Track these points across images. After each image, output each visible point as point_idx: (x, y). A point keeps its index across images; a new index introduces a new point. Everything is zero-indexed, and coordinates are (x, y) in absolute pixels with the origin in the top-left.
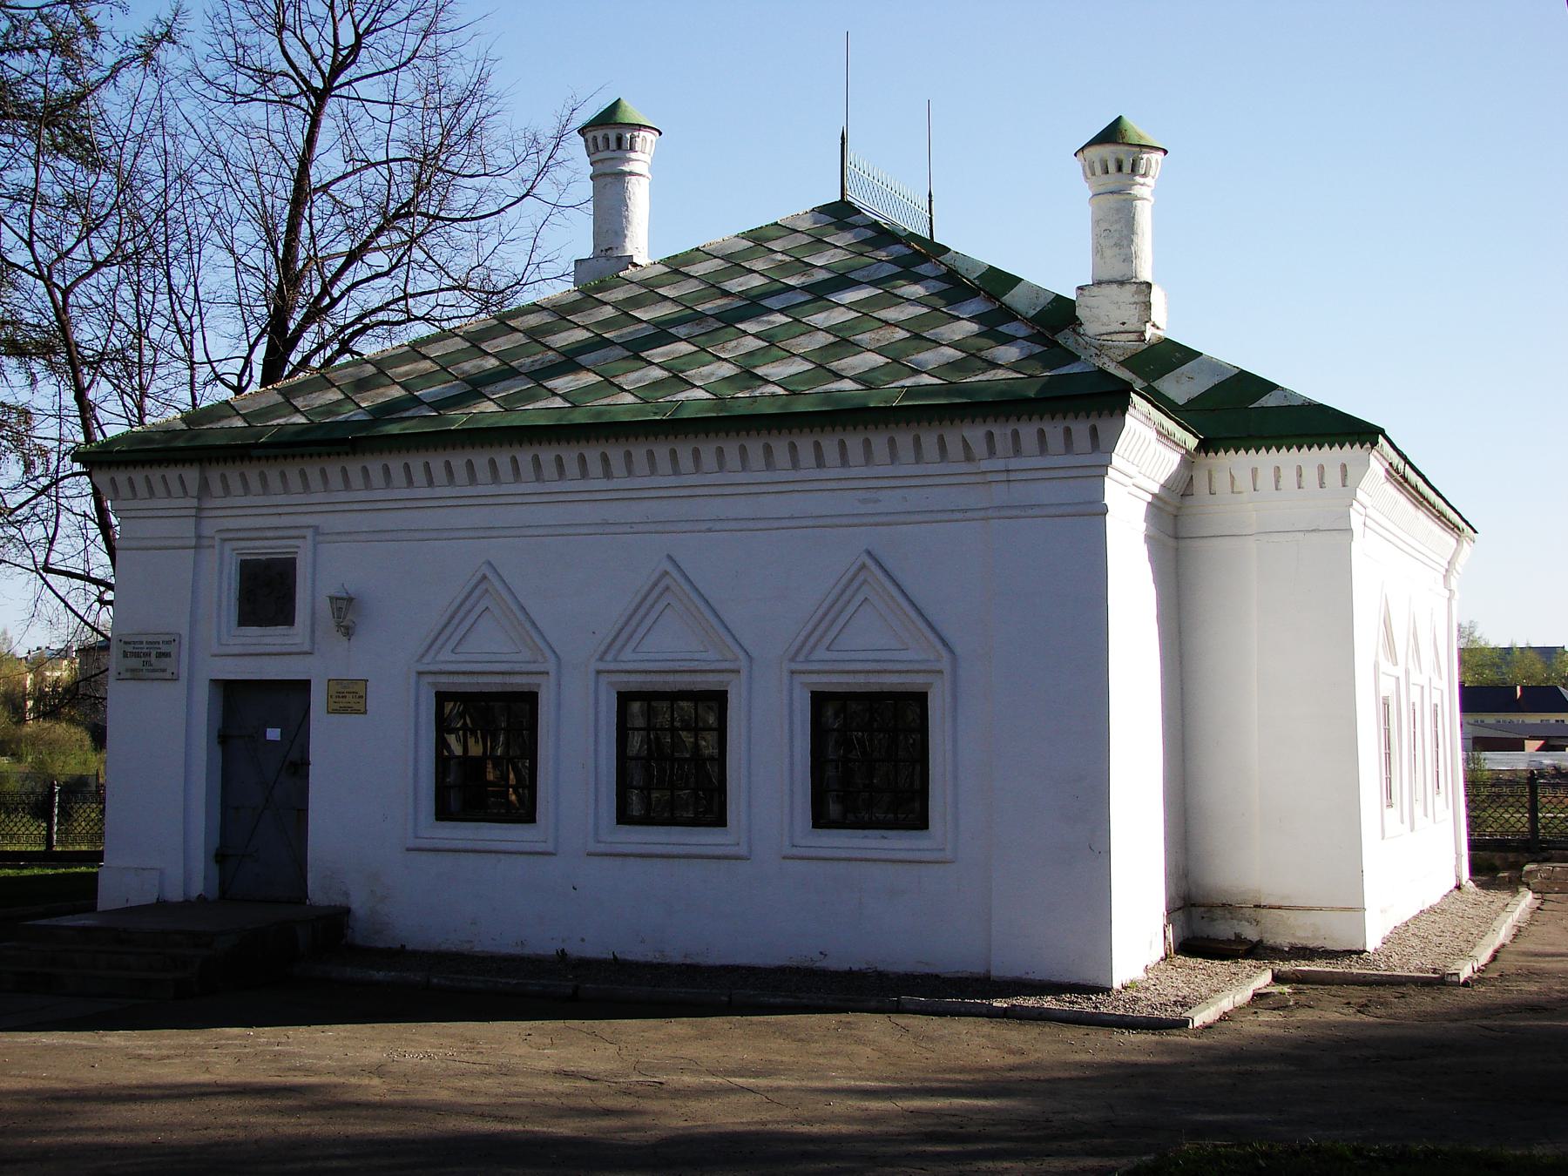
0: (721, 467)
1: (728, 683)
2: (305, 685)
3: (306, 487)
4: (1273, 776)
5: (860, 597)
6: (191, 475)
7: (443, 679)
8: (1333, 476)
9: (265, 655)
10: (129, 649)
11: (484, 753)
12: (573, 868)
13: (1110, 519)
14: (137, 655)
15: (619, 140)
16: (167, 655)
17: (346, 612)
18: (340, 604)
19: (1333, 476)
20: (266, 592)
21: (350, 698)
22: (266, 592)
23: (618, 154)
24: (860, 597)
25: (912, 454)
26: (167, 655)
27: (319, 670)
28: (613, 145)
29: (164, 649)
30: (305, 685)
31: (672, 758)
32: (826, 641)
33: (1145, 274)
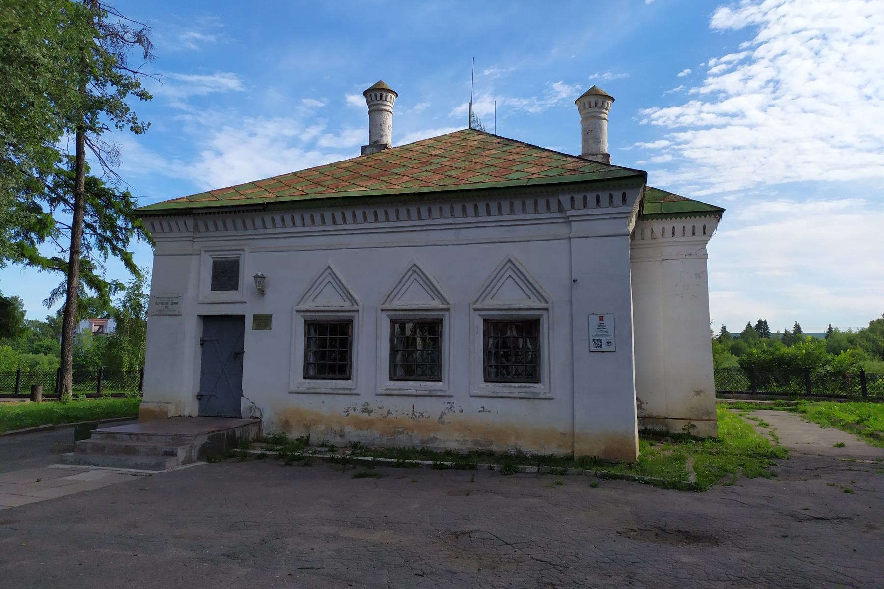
0: (376, 220)
1: (444, 315)
2: (242, 318)
3: (245, 228)
4: (764, 279)
5: (506, 276)
6: (190, 222)
7: (308, 314)
8: (699, 230)
9: (225, 303)
10: (158, 301)
11: (329, 347)
12: (371, 397)
13: (711, 239)
14: (163, 304)
15: (381, 96)
16: (176, 303)
17: (261, 285)
18: (259, 280)
19: (699, 230)
20: (225, 275)
21: (263, 322)
22: (225, 275)
23: (380, 102)
24: (506, 276)
25: (427, 214)
26: (176, 303)
27: (248, 312)
28: (378, 98)
29: (175, 300)
30: (242, 318)
31: (417, 347)
32: (491, 295)
33: (606, 151)
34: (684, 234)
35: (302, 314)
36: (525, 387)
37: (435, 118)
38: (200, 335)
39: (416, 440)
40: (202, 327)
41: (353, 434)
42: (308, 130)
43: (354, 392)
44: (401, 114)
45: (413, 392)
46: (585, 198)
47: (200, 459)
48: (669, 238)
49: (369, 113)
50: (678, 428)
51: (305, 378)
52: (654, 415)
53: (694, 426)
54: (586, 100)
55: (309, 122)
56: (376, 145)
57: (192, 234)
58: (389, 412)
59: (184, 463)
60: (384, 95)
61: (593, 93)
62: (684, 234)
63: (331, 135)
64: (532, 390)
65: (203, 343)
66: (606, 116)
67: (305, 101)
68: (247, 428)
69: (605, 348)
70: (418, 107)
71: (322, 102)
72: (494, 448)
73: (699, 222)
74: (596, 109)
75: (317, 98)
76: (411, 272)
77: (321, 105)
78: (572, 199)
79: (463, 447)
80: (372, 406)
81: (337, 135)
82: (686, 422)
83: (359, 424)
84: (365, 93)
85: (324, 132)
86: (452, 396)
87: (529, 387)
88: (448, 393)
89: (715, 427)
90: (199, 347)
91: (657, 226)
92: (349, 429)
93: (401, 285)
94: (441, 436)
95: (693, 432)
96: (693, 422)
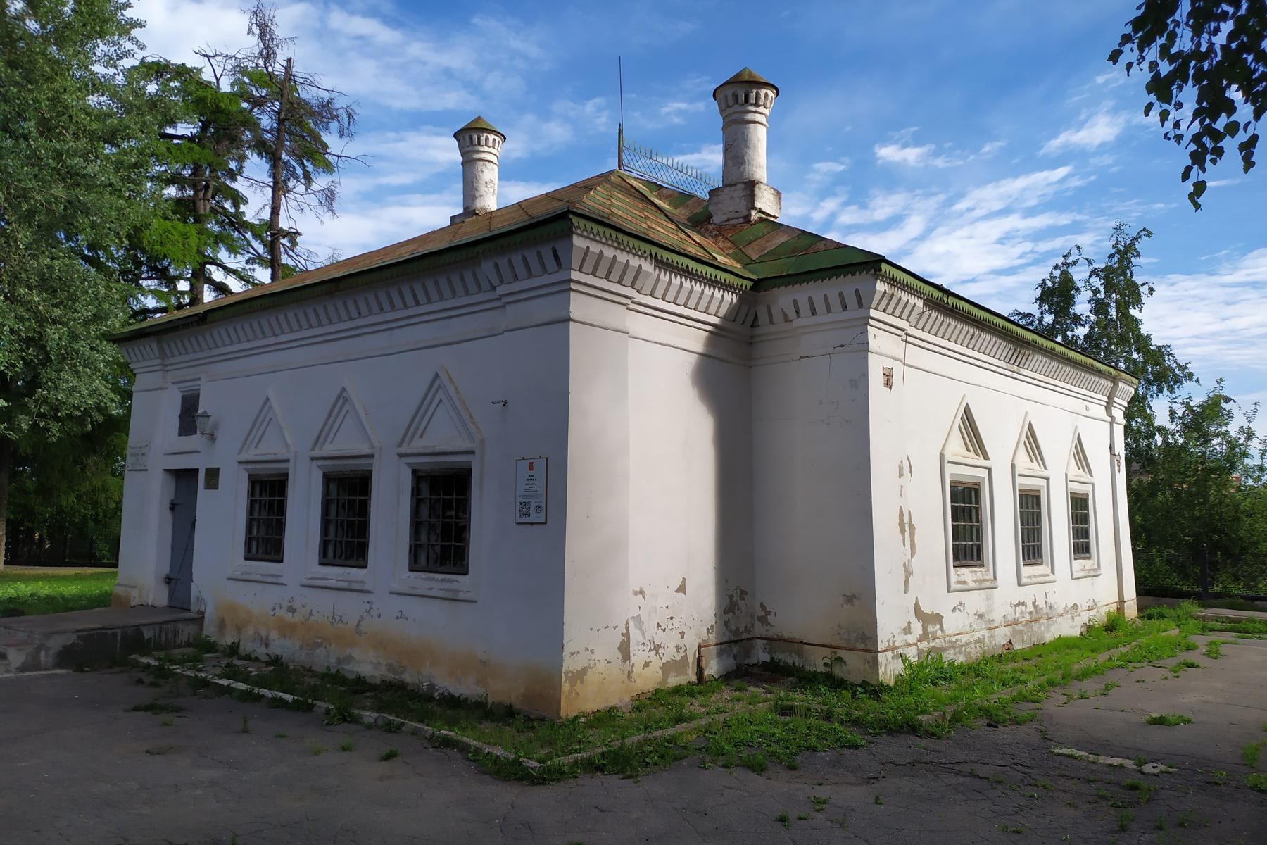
2: (197, 470)
7: (253, 466)
8: (851, 301)
32: (419, 434)
34: (829, 311)
35: (244, 466)
36: (449, 580)
37: (1015, 161)
38: (170, 494)
39: (324, 659)
40: (173, 485)
41: (282, 646)
42: (822, 204)
43: (280, 580)
44: (961, 163)
45: (332, 583)
46: (510, 262)
47: (59, 665)
48: (806, 320)
49: (463, 164)
50: (817, 661)
51: (246, 559)
52: (786, 635)
53: (840, 660)
54: (729, 92)
55: (825, 193)
56: (469, 212)
57: (159, 361)
58: (311, 614)
59: (22, 669)
60: (475, 137)
61: (736, 81)
62: (829, 311)
63: (853, 208)
64: (454, 586)
65: (173, 507)
66: (758, 118)
67: (817, 166)
68: (171, 626)
69: (534, 517)
70: (987, 148)
71: (842, 164)
72: (408, 678)
73: (847, 285)
74: (737, 108)
75: (835, 160)
76: (341, 401)
77: (841, 168)
78: (497, 266)
79: (377, 674)
80: (296, 605)
81: (864, 206)
82: (827, 651)
83: (286, 629)
84: (455, 136)
85: (846, 204)
86: (369, 592)
87: (449, 580)
88: (366, 587)
89: (875, 664)
90: (168, 516)
91: (783, 299)
92: (274, 635)
93: (332, 419)
94: (356, 653)
95: (838, 671)
96: (841, 653)
